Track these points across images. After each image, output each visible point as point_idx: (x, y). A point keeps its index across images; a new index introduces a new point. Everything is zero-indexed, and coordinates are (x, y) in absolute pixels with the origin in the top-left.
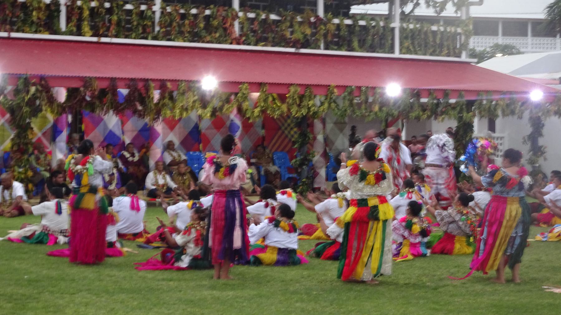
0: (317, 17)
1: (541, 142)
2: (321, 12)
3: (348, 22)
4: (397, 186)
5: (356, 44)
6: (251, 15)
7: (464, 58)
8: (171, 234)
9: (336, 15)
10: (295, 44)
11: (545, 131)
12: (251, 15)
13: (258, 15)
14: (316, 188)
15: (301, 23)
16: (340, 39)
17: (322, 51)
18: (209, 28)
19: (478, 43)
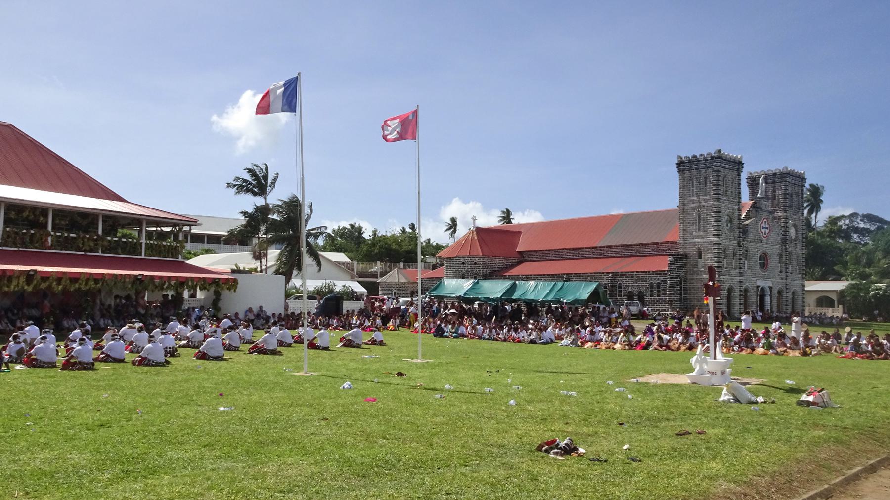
0: (98, 235)
1: (220, 304)
2: (100, 232)
3: (116, 239)
4: (171, 353)
5: (120, 251)
6: (58, 234)
7: (180, 259)
8: (510, 222)
9: (109, 235)
10: (85, 251)
11: (222, 297)
12: (58, 234)
13: (63, 234)
14: (314, 298)
15: (88, 239)
16: (111, 248)
17: (100, 254)
18: (31, 241)
19: (189, 246)
